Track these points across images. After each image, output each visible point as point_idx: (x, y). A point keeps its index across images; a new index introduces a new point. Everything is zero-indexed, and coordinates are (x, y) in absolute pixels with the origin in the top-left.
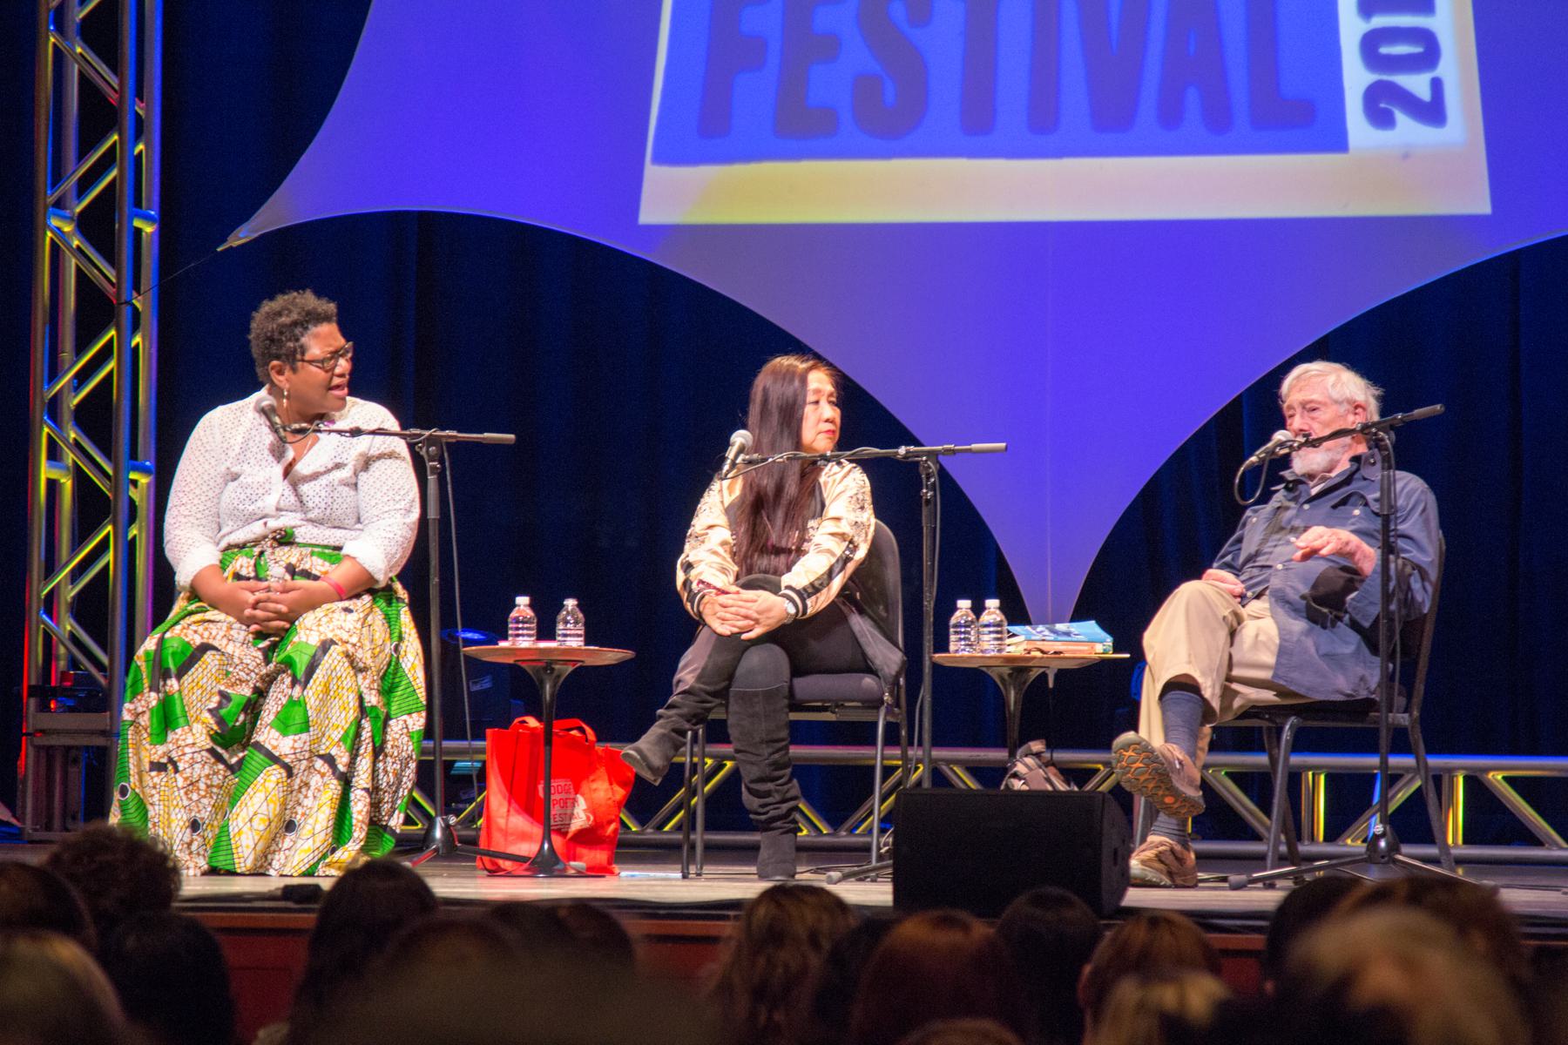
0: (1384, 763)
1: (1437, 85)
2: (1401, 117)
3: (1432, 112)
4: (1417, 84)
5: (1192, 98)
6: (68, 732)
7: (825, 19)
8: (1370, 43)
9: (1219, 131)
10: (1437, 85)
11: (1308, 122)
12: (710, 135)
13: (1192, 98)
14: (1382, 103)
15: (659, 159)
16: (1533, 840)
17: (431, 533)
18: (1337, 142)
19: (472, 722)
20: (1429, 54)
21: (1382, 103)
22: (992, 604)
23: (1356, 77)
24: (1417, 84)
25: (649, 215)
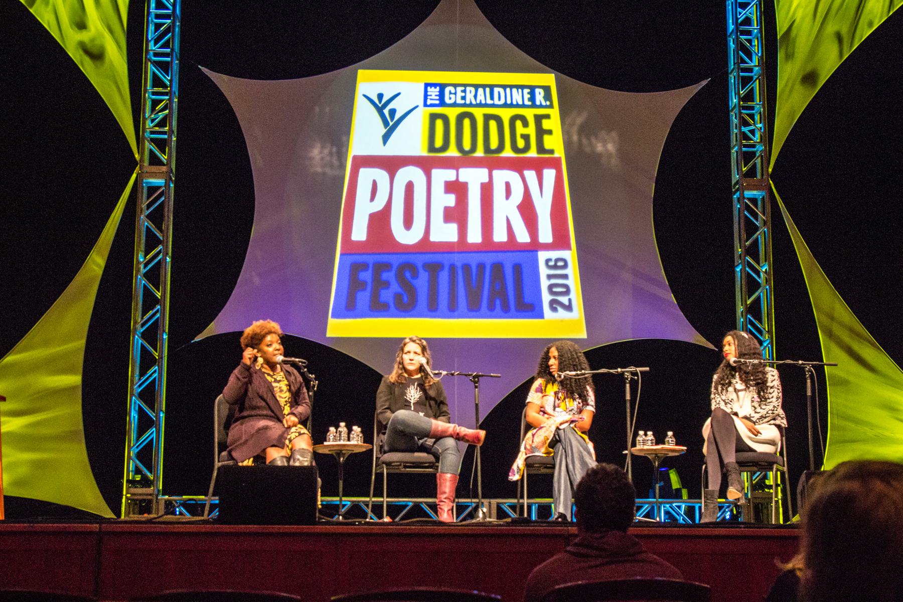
0: (341, 500)
1: (570, 300)
2: (559, 309)
3: (569, 308)
4: (564, 300)
5: (498, 302)
6: (140, 495)
7: (385, 276)
8: (550, 287)
9: (506, 312)
10: (570, 300)
11: (532, 309)
12: (349, 309)
13: (498, 302)
14: (554, 305)
15: (333, 317)
16: (757, 207)
17: (417, 454)
18: (541, 316)
19: (383, 484)
20: (567, 292)
21: (554, 305)
22: (356, 429)
23: (546, 298)
24: (564, 300)
25: (329, 334)
